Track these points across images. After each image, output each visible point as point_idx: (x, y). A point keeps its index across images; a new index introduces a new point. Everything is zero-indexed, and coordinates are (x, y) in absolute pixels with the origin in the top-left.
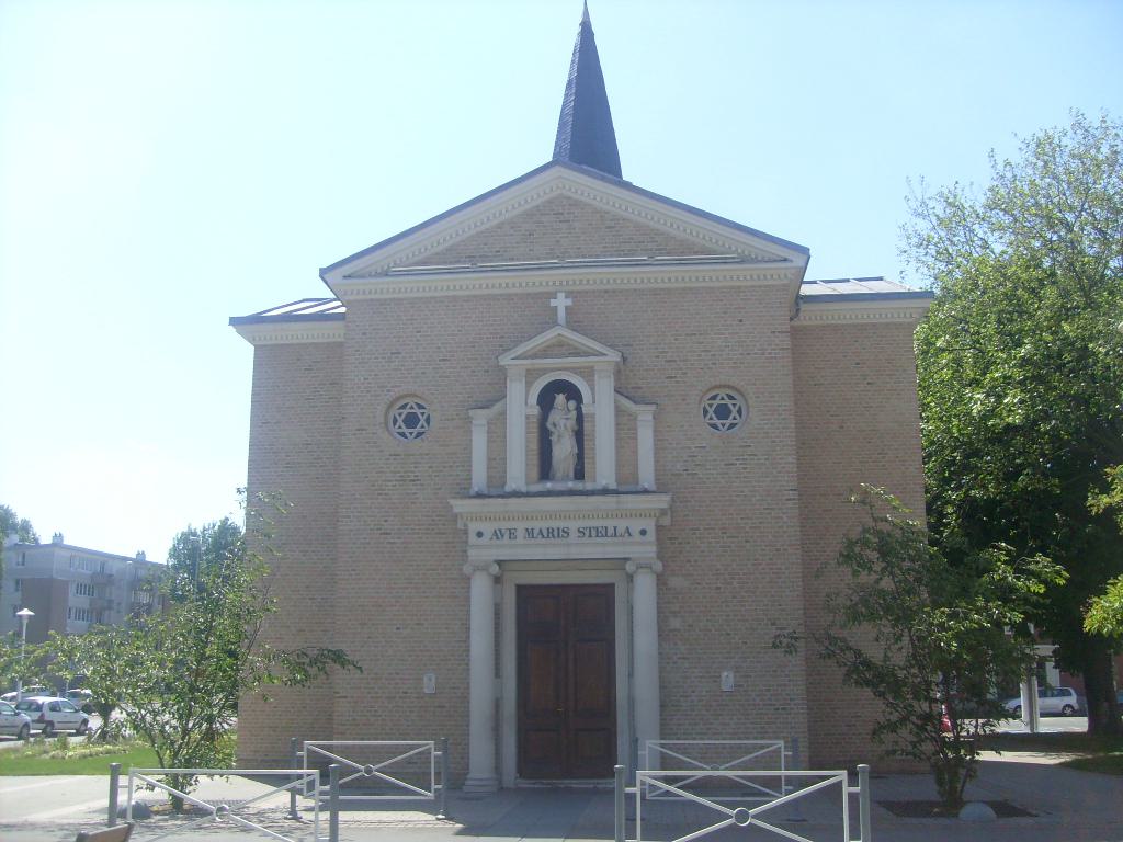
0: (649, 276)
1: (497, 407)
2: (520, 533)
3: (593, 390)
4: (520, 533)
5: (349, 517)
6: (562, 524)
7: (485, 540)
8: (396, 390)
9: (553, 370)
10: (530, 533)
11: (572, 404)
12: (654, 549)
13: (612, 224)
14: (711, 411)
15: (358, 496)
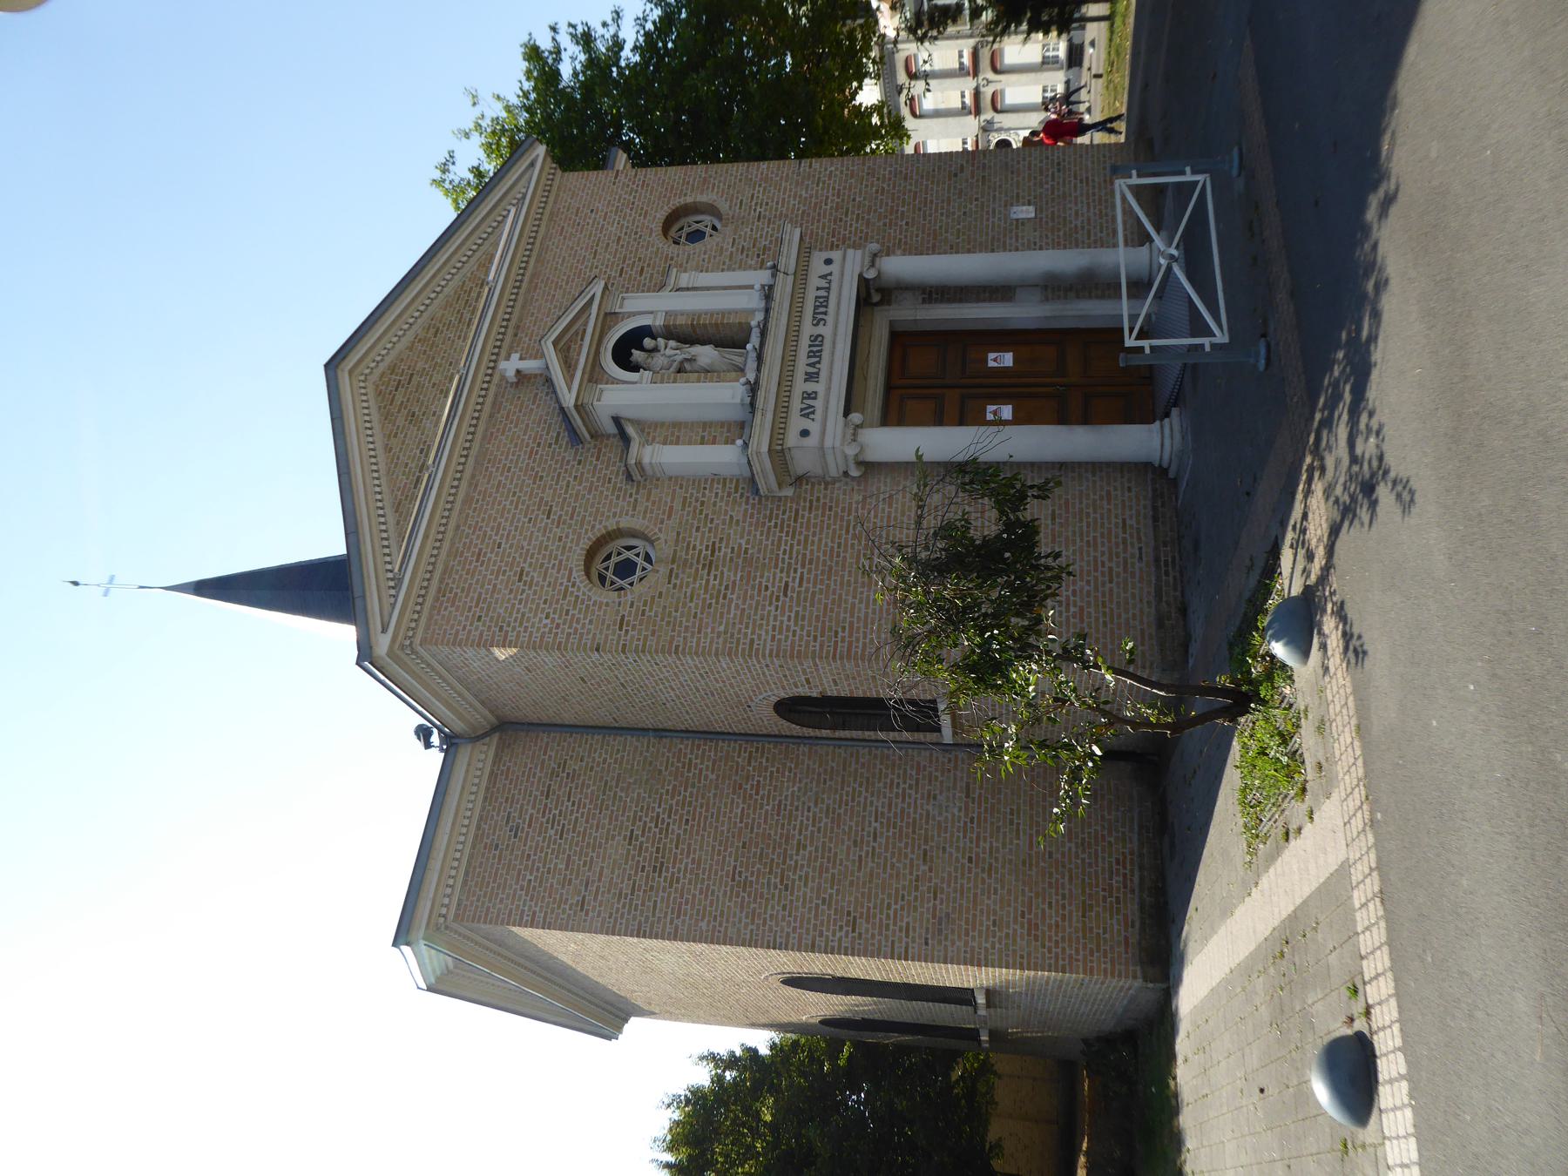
0: (403, 627)
1: (631, 430)
2: (810, 387)
3: (634, 314)
4: (806, 424)
5: (752, 641)
6: (805, 342)
7: (814, 427)
8: (574, 574)
9: (597, 353)
10: (811, 377)
11: (648, 342)
12: (850, 252)
13: (432, 331)
14: (609, 574)
15: (722, 628)
